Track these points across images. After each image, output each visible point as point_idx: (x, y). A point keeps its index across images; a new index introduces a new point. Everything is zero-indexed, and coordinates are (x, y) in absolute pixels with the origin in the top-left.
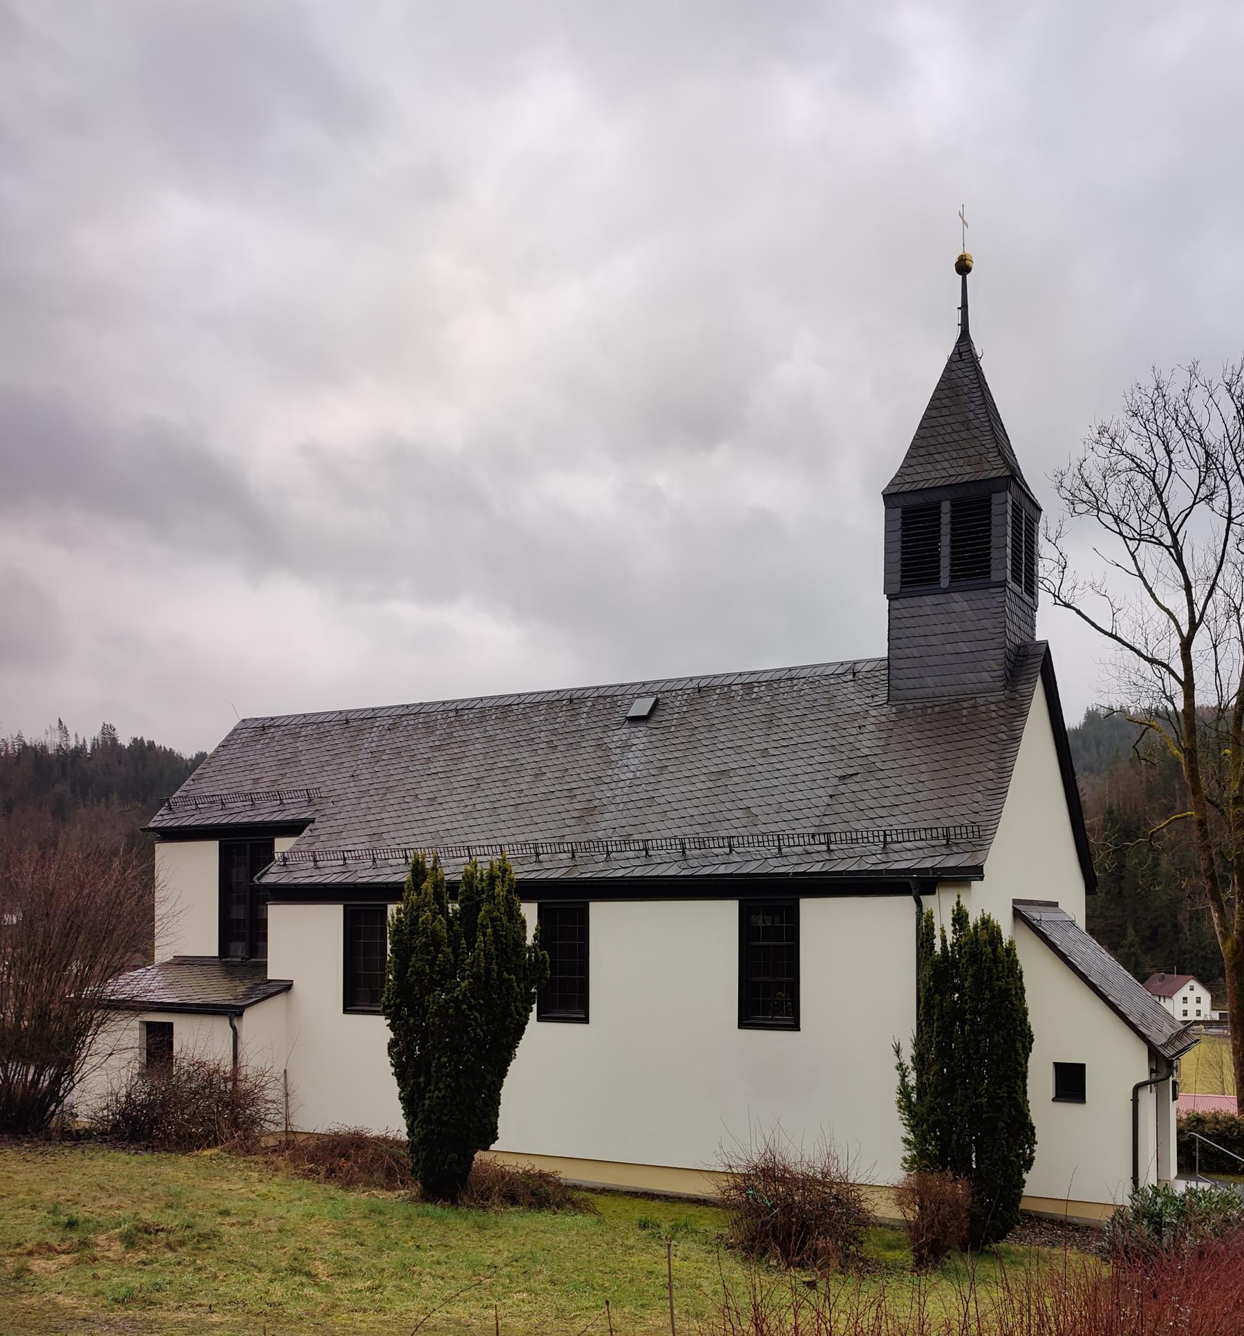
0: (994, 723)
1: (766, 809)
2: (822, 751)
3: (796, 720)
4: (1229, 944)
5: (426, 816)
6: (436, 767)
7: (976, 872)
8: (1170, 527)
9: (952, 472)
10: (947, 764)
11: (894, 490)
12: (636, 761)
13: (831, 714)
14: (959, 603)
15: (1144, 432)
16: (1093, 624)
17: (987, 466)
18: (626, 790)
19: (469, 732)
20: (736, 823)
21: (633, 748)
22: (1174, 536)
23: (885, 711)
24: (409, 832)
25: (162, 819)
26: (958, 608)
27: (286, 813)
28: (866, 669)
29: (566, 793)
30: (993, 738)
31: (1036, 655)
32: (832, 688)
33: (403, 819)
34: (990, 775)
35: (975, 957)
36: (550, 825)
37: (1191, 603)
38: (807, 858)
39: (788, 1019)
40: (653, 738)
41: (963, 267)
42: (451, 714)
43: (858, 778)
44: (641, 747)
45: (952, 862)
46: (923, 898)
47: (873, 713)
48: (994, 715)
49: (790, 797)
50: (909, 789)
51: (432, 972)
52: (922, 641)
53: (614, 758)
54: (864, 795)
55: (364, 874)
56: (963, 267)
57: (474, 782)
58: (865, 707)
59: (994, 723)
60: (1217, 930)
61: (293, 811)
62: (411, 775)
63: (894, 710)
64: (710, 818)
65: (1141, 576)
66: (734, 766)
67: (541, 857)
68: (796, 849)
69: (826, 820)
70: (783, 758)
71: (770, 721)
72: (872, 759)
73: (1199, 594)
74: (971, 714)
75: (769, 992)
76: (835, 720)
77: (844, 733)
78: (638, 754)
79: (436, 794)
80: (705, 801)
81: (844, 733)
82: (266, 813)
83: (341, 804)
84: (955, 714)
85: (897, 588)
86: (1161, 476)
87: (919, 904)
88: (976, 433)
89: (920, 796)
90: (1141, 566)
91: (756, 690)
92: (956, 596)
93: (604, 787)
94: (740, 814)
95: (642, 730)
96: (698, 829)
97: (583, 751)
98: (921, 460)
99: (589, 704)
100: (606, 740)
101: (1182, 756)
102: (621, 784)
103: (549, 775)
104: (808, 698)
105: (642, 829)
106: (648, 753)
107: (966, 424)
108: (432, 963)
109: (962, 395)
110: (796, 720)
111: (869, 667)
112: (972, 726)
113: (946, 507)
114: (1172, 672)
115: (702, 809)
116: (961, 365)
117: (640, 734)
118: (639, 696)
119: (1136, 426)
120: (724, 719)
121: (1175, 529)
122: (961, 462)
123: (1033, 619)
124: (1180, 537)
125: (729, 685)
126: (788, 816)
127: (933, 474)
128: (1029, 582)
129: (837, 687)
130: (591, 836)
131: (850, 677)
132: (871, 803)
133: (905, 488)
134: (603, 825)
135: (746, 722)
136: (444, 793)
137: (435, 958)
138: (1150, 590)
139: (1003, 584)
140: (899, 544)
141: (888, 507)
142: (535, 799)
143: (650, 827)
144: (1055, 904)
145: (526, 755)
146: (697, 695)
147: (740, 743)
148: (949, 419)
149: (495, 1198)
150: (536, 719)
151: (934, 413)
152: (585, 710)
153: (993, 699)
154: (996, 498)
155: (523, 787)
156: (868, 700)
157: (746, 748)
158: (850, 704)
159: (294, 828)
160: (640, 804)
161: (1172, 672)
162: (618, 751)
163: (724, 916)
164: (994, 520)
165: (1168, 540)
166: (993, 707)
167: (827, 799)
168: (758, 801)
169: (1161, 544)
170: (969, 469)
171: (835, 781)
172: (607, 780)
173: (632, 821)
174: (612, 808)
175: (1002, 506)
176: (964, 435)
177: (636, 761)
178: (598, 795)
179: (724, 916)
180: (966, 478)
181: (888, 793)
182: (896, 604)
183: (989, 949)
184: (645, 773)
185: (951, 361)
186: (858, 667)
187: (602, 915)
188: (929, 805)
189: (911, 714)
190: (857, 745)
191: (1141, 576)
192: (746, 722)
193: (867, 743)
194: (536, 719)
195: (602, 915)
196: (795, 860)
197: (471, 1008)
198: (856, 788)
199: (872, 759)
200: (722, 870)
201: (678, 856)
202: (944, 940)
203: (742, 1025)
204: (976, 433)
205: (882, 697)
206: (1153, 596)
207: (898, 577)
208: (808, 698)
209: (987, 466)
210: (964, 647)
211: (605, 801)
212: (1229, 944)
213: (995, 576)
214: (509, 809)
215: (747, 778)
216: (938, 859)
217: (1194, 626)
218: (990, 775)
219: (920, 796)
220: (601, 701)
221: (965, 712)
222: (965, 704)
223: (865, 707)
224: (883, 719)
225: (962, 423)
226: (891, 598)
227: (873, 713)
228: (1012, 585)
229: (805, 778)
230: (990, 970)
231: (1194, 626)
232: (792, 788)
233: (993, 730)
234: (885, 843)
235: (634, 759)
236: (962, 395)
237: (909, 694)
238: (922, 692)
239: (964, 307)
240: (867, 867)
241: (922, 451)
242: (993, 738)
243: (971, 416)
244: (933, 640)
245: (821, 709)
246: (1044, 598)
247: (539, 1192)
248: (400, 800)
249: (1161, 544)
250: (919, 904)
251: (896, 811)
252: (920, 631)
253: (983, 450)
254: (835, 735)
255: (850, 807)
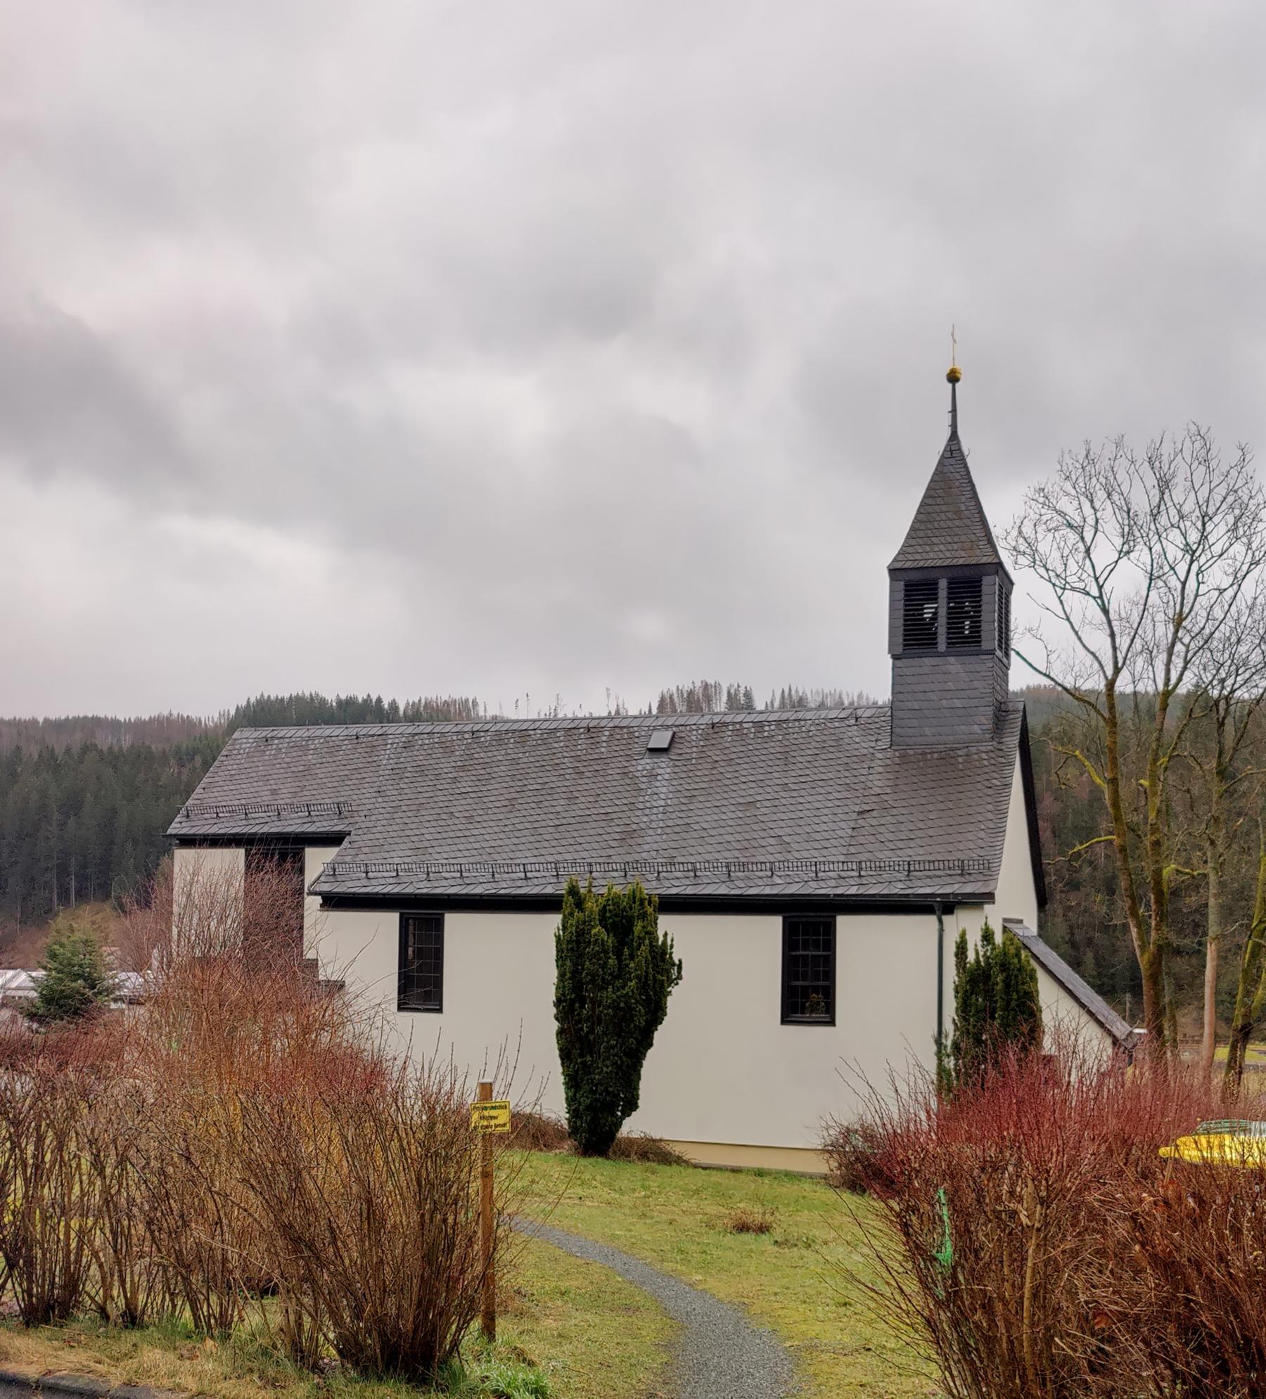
0: (986, 770)
1: (797, 838)
2: (838, 788)
3: (809, 758)
4: (1146, 956)
5: (467, 833)
6: (464, 786)
7: (989, 897)
8: (1097, 579)
9: (948, 554)
10: (950, 805)
11: (899, 565)
12: (664, 790)
13: (840, 755)
14: (954, 665)
15: (1073, 492)
16: (1030, 665)
17: (978, 552)
18: (660, 816)
19: (490, 754)
20: (770, 849)
21: (659, 778)
22: (1100, 588)
23: (889, 755)
24: (454, 848)
25: (176, 828)
26: (955, 669)
27: (318, 824)
28: (866, 715)
29: (603, 817)
30: (987, 783)
31: (1016, 711)
32: (837, 731)
33: (444, 835)
34: (990, 816)
35: (1004, 967)
36: (595, 846)
37: (1115, 648)
38: (842, 882)
39: (824, 1017)
40: (677, 770)
41: (953, 378)
42: (467, 736)
43: (875, 814)
44: (667, 777)
45: (969, 889)
46: (945, 918)
47: (879, 756)
48: (986, 763)
49: (817, 828)
50: (921, 825)
51: (605, 973)
52: (921, 696)
53: (643, 786)
54: (881, 829)
55: (423, 888)
56: (953, 378)
57: (507, 803)
58: (871, 750)
59: (986, 770)
60: (1136, 944)
61: (325, 824)
62: (439, 793)
63: (897, 754)
64: (746, 844)
65: (1068, 619)
66: (759, 798)
67: (594, 875)
68: (831, 874)
69: (852, 850)
70: (803, 793)
71: (786, 758)
72: (885, 797)
73: (1123, 642)
74: (965, 761)
75: (808, 991)
76: (846, 760)
77: (855, 773)
78: (664, 783)
79: (473, 813)
80: (738, 829)
81: (855, 773)
82: (293, 825)
83: (373, 818)
84: (953, 761)
85: (899, 650)
86: (1088, 535)
87: (941, 921)
88: (968, 522)
89: (931, 832)
90: (1068, 611)
91: (766, 728)
92: (952, 659)
93: (639, 813)
94: (773, 841)
95: (663, 760)
96: (737, 854)
97: (610, 778)
98: (920, 541)
99: (607, 733)
100: (631, 769)
101: (1105, 786)
102: (655, 811)
103: (583, 799)
104: (817, 739)
105: (684, 852)
106: (674, 783)
107: (958, 512)
108: (604, 966)
109: (952, 491)
110: (809, 758)
111: (868, 713)
112: (968, 772)
113: (943, 584)
114: (1098, 712)
115: (738, 837)
116: (952, 461)
117: (663, 765)
118: (655, 729)
119: (1068, 486)
120: (741, 755)
121: (1101, 581)
122: (956, 547)
123: (1007, 675)
124: (1107, 589)
125: (741, 723)
126: (817, 845)
127: (931, 555)
128: (1006, 650)
129: (842, 730)
130: (637, 857)
131: (853, 722)
132: (891, 836)
133: (908, 565)
134: (646, 847)
135: (763, 758)
136: (481, 812)
137: (605, 963)
138: (1076, 633)
139: (992, 652)
140: (902, 612)
141: (892, 579)
142: (572, 821)
143: (692, 850)
144: (1021, 921)
145: (554, 779)
146: (711, 731)
147: (761, 777)
148: (944, 508)
149: (634, 1157)
150: (556, 745)
151: (930, 501)
152: (604, 739)
153: (983, 749)
154: (986, 580)
155: (559, 809)
156: (873, 744)
157: (768, 782)
158: (857, 746)
159: (333, 839)
160: (677, 829)
161: (1098, 712)
162: (644, 779)
163: (390, 921)
164: (984, 598)
165: (1095, 592)
166: (984, 756)
167: (850, 831)
168: (788, 830)
169: (1088, 594)
170: (963, 554)
171: (855, 816)
172: (641, 806)
173: (673, 845)
174: (651, 832)
175: (990, 585)
176: (957, 523)
177: (664, 790)
178: (634, 820)
179: (390, 921)
180: (961, 561)
181: (902, 827)
182: (899, 663)
183: (1016, 960)
184: (676, 801)
185: (943, 457)
186: (859, 712)
187: (454, 923)
188: (940, 840)
189: (912, 759)
190: (869, 784)
191: (1068, 619)
192: (763, 758)
193: (878, 783)
194: (556, 745)
195: (454, 923)
196: (833, 883)
197: (637, 1002)
198: (874, 822)
199: (885, 797)
200: (768, 891)
201: (724, 878)
202: (977, 953)
203: (784, 1021)
204: (968, 522)
205: (885, 743)
206: (1079, 638)
207: (900, 640)
208: (817, 739)
209: (978, 552)
210: (958, 703)
211: (643, 826)
212: (1146, 956)
213: (985, 645)
214: (550, 829)
215: (775, 810)
216: (956, 886)
217: (1117, 670)
218: (990, 816)
219: (931, 832)
220: (618, 731)
221: (960, 760)
222: (960, 753)
223: (871, 750)
224: (889, 762)
225: (955, 513)
226: (895, 657)
227: (879, 756)
228: (998, 653)
229: (826, 811)
230: (1016, 976)
231: (1117, 670)
232: (816, 820)
233: (986, 776)
234: (909, 871)
235: (662, 787)
236: (952, 491)
237: (910, 741)
238: (920, 740)
239: (954, 411)
240: (896, 891)
241: (921, 534)
242: (987, 783)
243: (963, 508)
244: (932, 696)
245: (831, 749)
246: (1013, 654)
247: (653, 1153)
248: (436, 817)
249: (1088, 594)
250: (941, 921)
251: (912, 844)
252: (921, 688)
253: (973, 538)
254: (847, 774)
255: (872, 839)
